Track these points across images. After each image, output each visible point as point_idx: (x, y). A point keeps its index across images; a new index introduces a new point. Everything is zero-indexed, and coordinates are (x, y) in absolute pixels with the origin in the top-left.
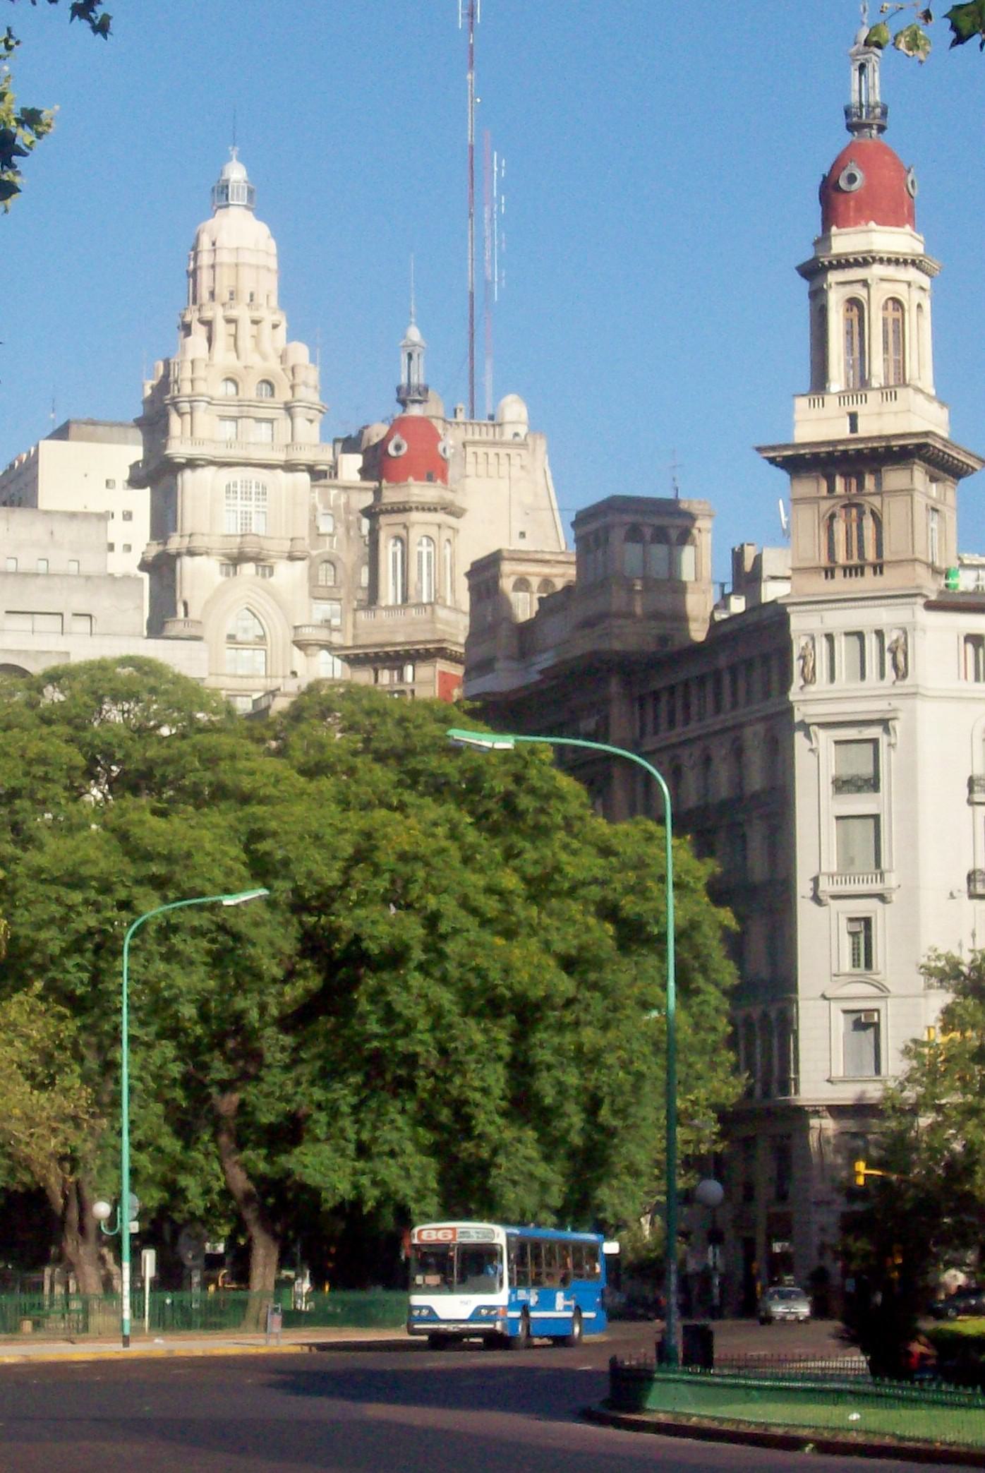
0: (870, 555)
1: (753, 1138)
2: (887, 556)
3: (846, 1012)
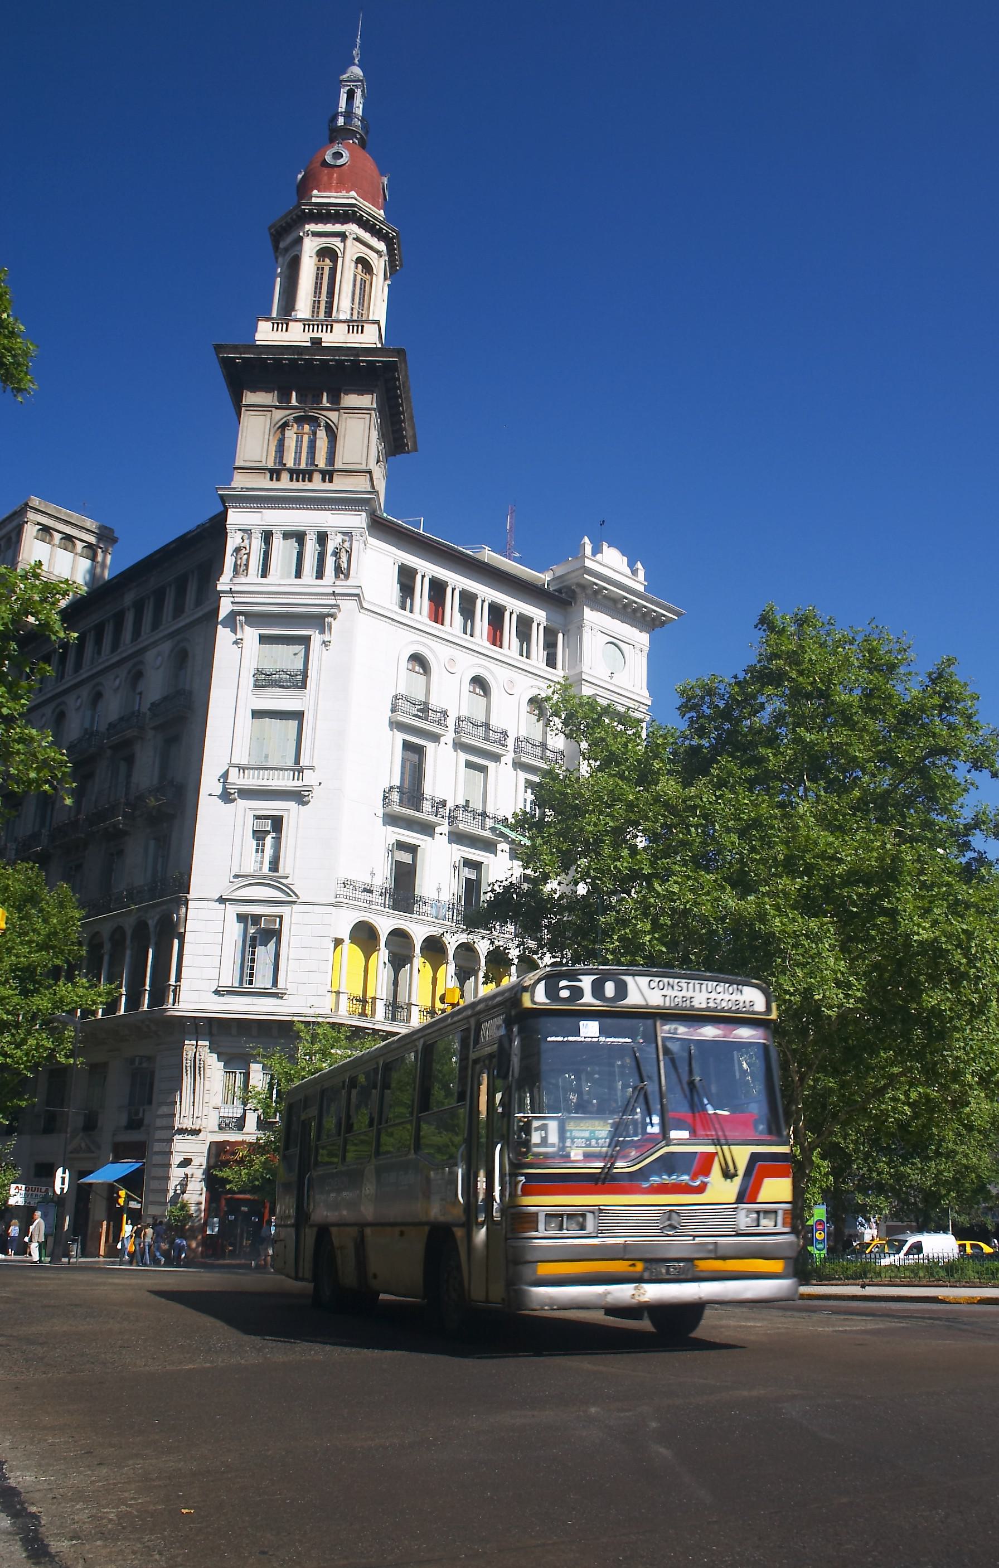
0: (321, 462)
1: (105, 1065)
2: (338, 465)
3: (241, 918)
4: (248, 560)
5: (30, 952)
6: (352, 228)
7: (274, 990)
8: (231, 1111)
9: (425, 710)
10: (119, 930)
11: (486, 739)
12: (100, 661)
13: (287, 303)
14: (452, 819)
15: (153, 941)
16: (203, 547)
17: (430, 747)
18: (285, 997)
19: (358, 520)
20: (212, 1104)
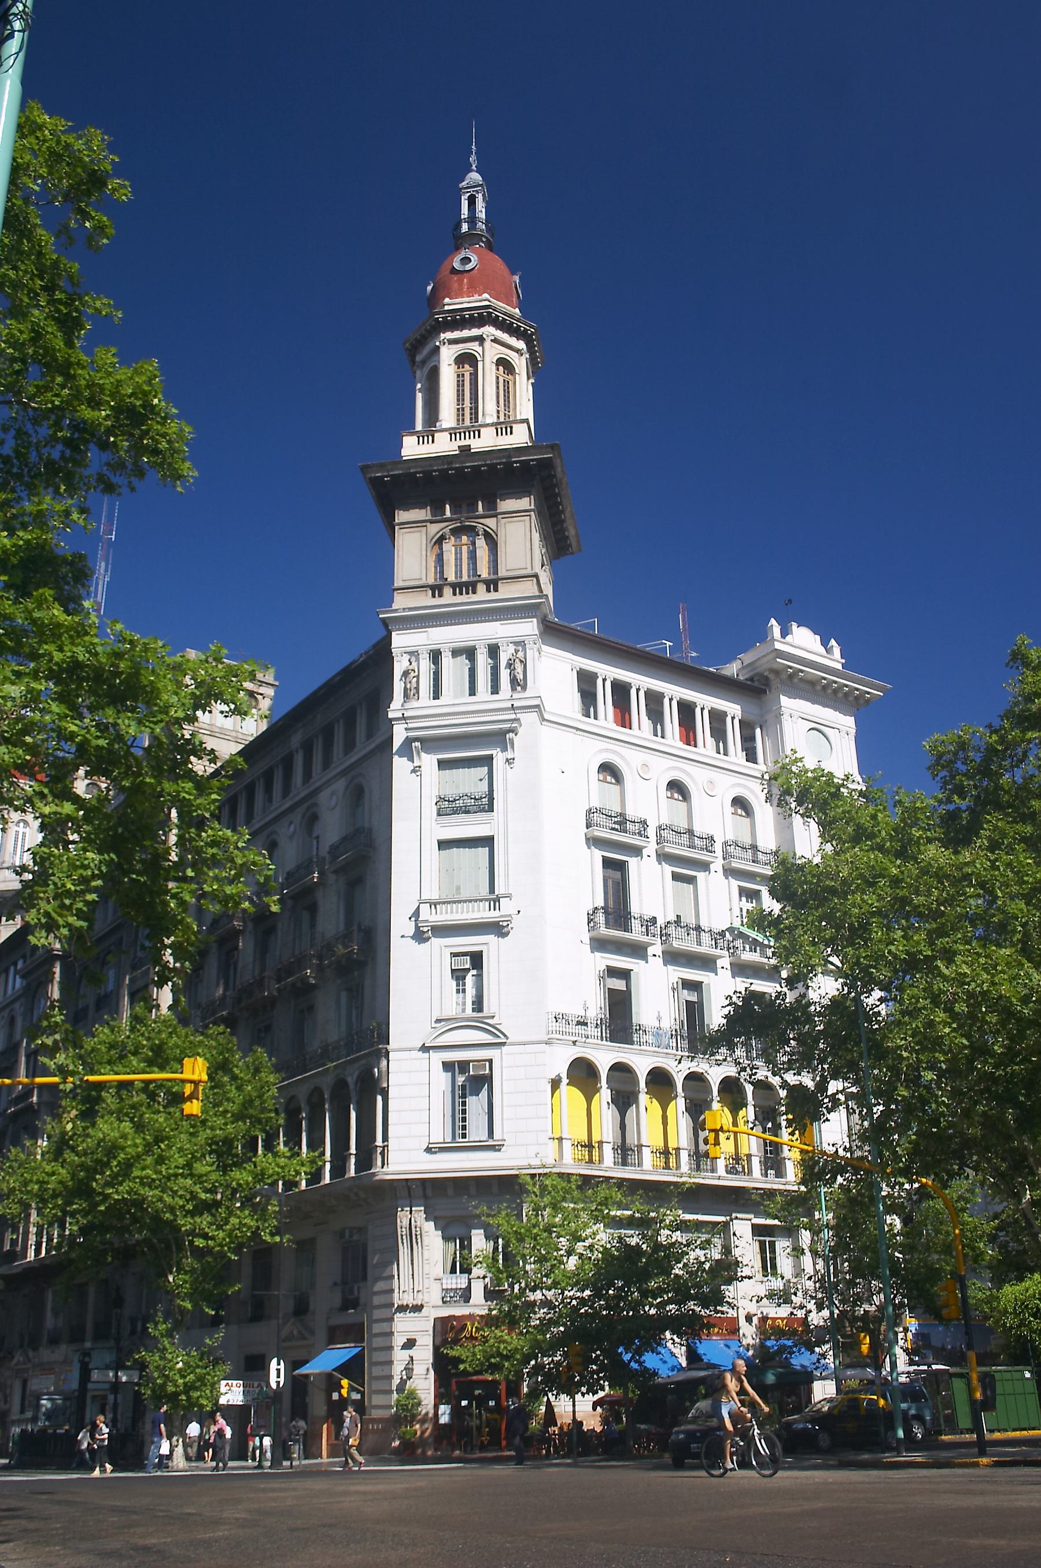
0: (484, 572)
1: (312, 1241)
2: (502, 573)
3: (448, 1066)
4: (418, 682)
5: (226, 1124)
6: (489, 331)
7: (491, 1143)
8: (454, 1281)
9: (622, 822)
10: (318, 1091)
11: (692, 846)
12: (273, 808)
14: (665, 936)
15: (354, 1100)
16: (368, 678)
17: (633, 862)
18: (503, 1149)
19: (529, 628)
20: (433, 1275)
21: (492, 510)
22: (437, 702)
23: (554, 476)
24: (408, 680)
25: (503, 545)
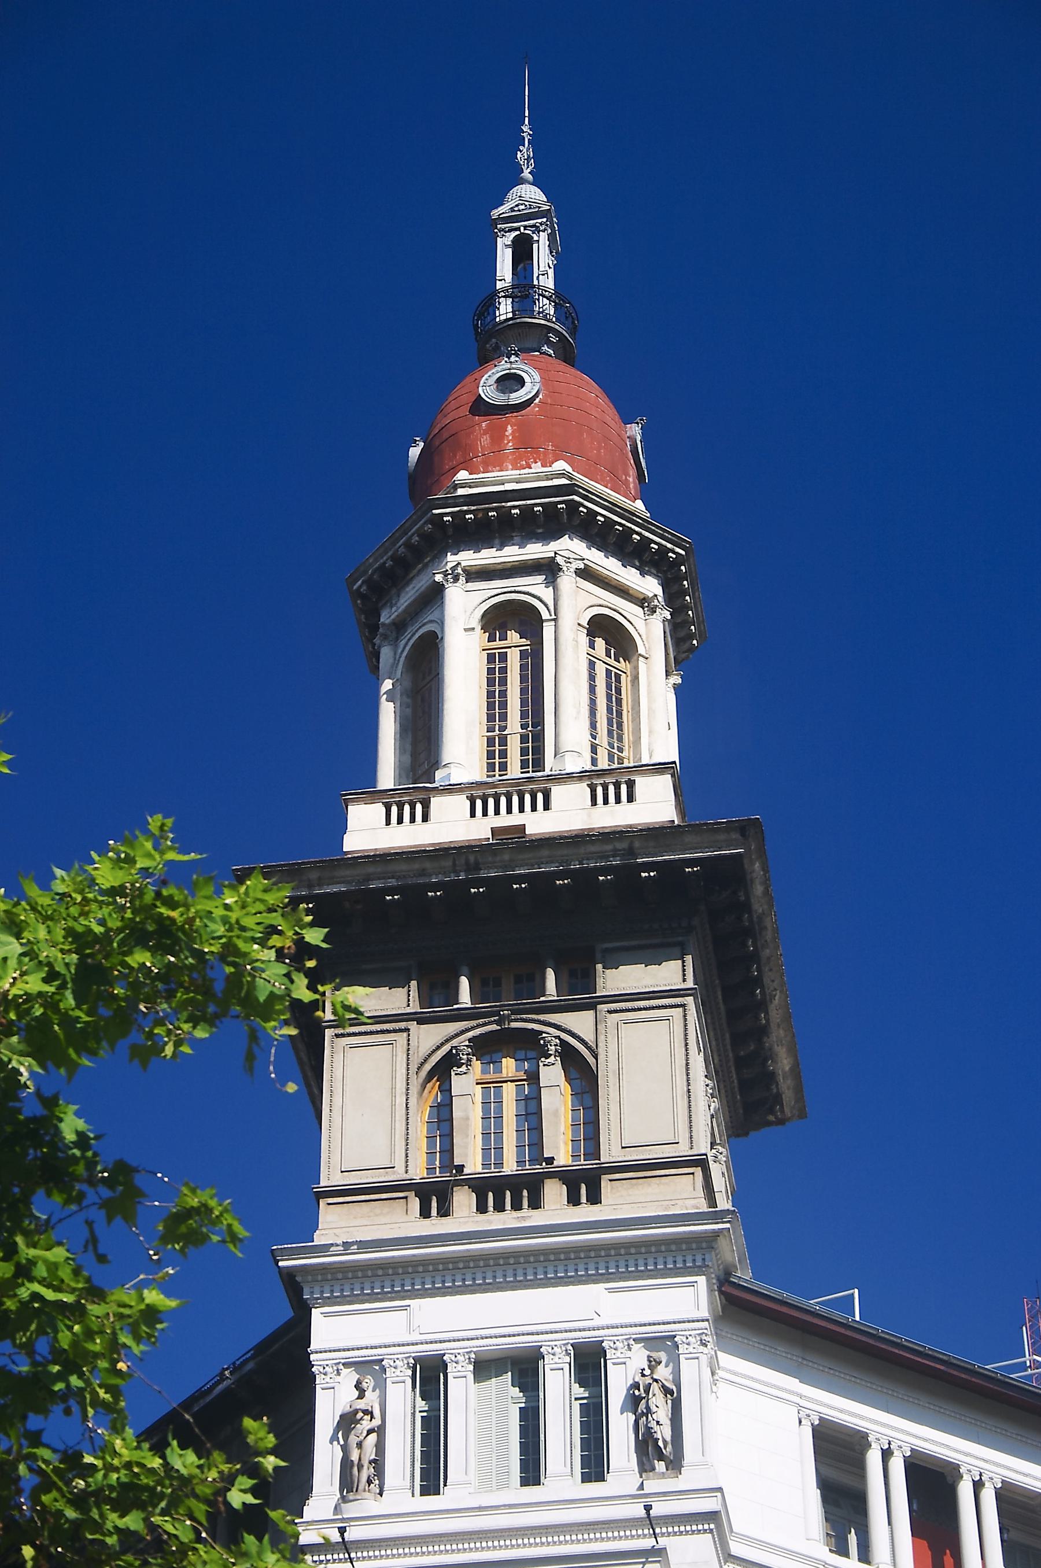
0: (560, 1147)
2: (611, 1152)
4: (380, 1447)
6: (570, 548)
13: (414, 755)
19: (683, 1301)
21: (580, 992)
22: (431, 1502)
23: (746, 907)
24: (353, 1440)
25: (613, 1080)
